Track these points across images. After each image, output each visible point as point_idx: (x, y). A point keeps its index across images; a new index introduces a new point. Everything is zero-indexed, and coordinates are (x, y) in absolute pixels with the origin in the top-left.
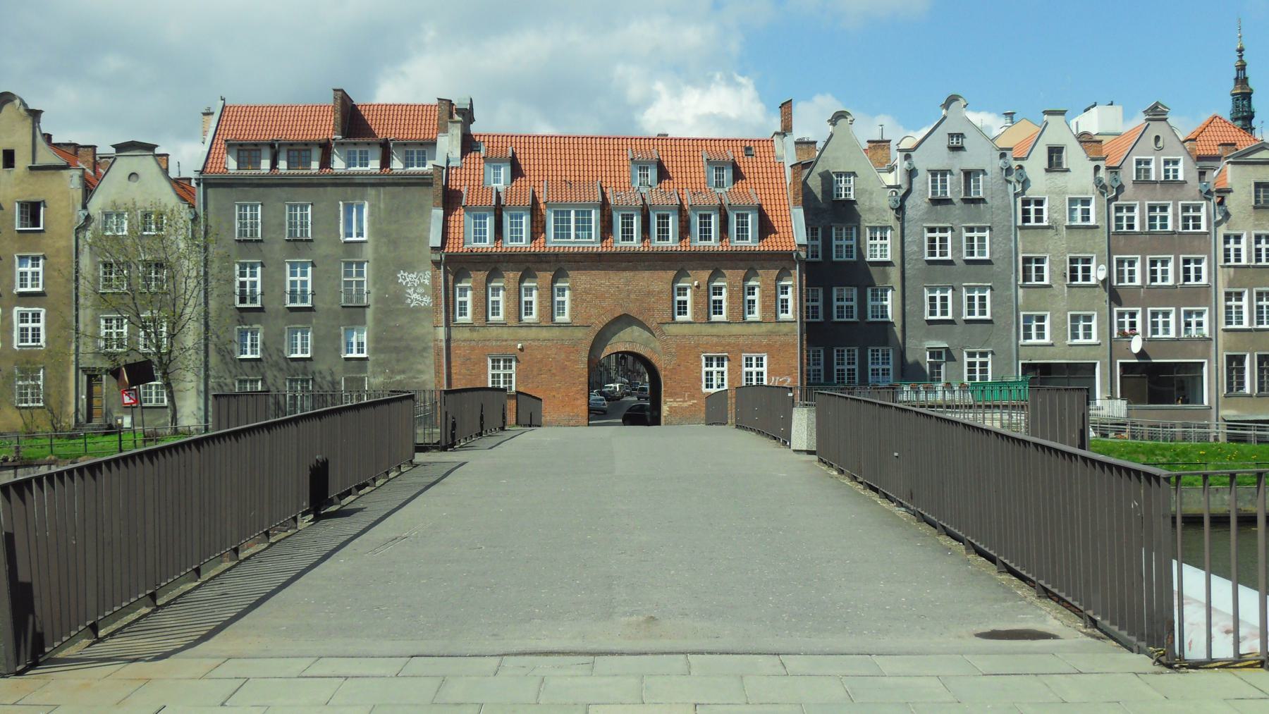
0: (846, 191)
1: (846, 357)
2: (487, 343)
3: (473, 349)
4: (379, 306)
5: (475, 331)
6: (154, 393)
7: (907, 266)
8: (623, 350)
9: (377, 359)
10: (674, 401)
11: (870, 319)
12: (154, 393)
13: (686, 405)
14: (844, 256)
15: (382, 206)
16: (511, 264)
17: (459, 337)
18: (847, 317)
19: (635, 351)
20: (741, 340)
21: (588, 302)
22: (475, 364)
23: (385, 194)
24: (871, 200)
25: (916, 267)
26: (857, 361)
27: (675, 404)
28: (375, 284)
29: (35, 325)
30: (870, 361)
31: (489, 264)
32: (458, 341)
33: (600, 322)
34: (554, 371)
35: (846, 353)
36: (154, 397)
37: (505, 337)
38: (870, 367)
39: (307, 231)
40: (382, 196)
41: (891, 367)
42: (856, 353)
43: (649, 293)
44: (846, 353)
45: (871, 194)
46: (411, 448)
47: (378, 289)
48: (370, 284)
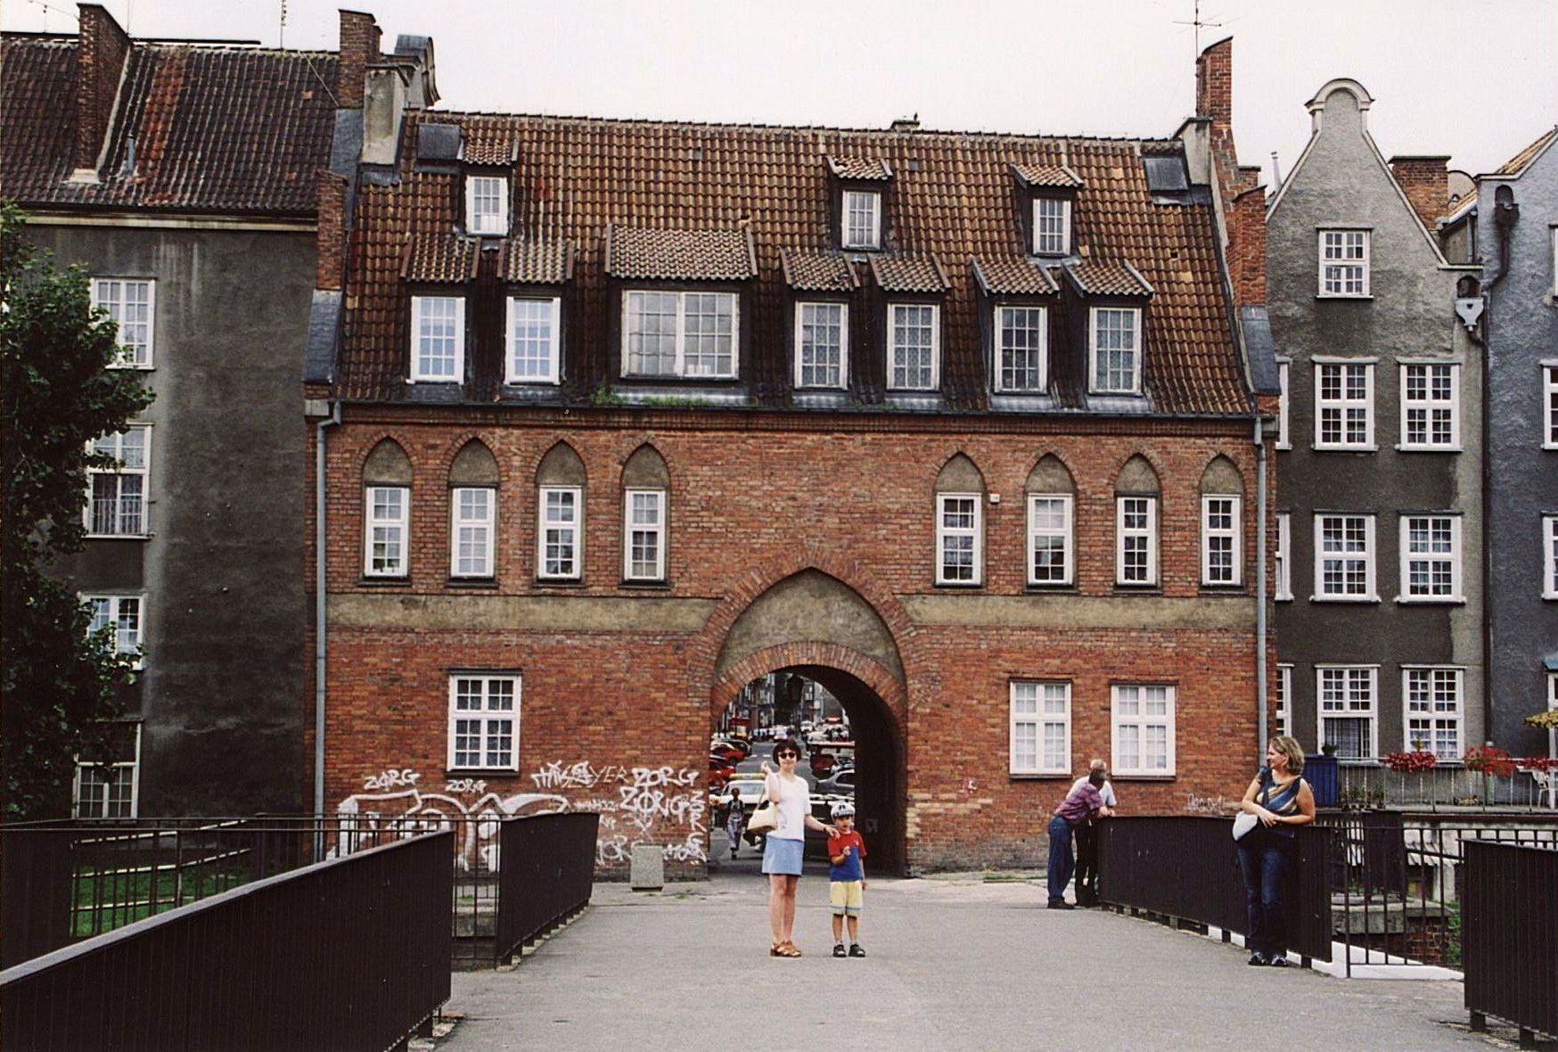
0: (1349, 275)
1: (1347, 690)
2: (449, 639)
3: (408, 652)
4: (176, 540)
5: (415, 604)
6: (484, 743)
7: (1498, 464)
8: (804, 661)
9: (168, 676)
10: (935, 799)
11: (1320, 594)
12: (484, 743)
13: (963, 809)
14: (118, 528)
15: (195, 288)
16: (517, 432)
17: (372, 622)
18: (1351, 589)
19: (835, 665)
20: (1109, 644)
21: (717, 535)
22: (415, 692)
23: (203, 257)
24: (1411, 298)
25: (1522, 467)
26: (1374, 700)
27: (937, 808)
28: (170, 483)
29: (1441, 404)
30: (1407, 700)
31: (458, 431)
32: (371, 629)
33: (747, 590)
34: (621, 715)
35: (1347, 679)
36: (484, 750)
37: (496, 622)
38: (1408, 715)
39: (1043, 212)
40: (196, 260)
41: (1458, 715)
42: (1373, 678)
43: (875, 517)
44: (1347, 679)
45: (1412, 282)
46: (1224, 947)
47: (178, 497)
48: (159, 484)
